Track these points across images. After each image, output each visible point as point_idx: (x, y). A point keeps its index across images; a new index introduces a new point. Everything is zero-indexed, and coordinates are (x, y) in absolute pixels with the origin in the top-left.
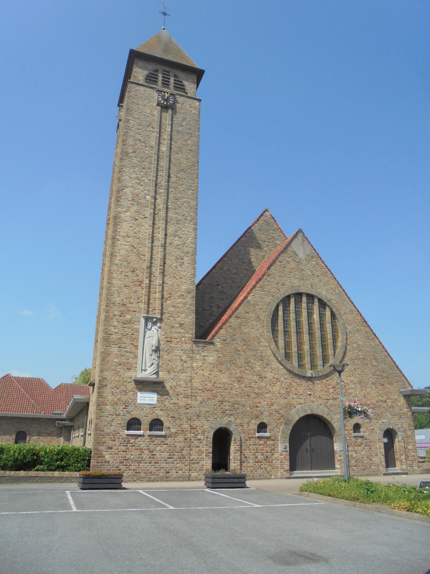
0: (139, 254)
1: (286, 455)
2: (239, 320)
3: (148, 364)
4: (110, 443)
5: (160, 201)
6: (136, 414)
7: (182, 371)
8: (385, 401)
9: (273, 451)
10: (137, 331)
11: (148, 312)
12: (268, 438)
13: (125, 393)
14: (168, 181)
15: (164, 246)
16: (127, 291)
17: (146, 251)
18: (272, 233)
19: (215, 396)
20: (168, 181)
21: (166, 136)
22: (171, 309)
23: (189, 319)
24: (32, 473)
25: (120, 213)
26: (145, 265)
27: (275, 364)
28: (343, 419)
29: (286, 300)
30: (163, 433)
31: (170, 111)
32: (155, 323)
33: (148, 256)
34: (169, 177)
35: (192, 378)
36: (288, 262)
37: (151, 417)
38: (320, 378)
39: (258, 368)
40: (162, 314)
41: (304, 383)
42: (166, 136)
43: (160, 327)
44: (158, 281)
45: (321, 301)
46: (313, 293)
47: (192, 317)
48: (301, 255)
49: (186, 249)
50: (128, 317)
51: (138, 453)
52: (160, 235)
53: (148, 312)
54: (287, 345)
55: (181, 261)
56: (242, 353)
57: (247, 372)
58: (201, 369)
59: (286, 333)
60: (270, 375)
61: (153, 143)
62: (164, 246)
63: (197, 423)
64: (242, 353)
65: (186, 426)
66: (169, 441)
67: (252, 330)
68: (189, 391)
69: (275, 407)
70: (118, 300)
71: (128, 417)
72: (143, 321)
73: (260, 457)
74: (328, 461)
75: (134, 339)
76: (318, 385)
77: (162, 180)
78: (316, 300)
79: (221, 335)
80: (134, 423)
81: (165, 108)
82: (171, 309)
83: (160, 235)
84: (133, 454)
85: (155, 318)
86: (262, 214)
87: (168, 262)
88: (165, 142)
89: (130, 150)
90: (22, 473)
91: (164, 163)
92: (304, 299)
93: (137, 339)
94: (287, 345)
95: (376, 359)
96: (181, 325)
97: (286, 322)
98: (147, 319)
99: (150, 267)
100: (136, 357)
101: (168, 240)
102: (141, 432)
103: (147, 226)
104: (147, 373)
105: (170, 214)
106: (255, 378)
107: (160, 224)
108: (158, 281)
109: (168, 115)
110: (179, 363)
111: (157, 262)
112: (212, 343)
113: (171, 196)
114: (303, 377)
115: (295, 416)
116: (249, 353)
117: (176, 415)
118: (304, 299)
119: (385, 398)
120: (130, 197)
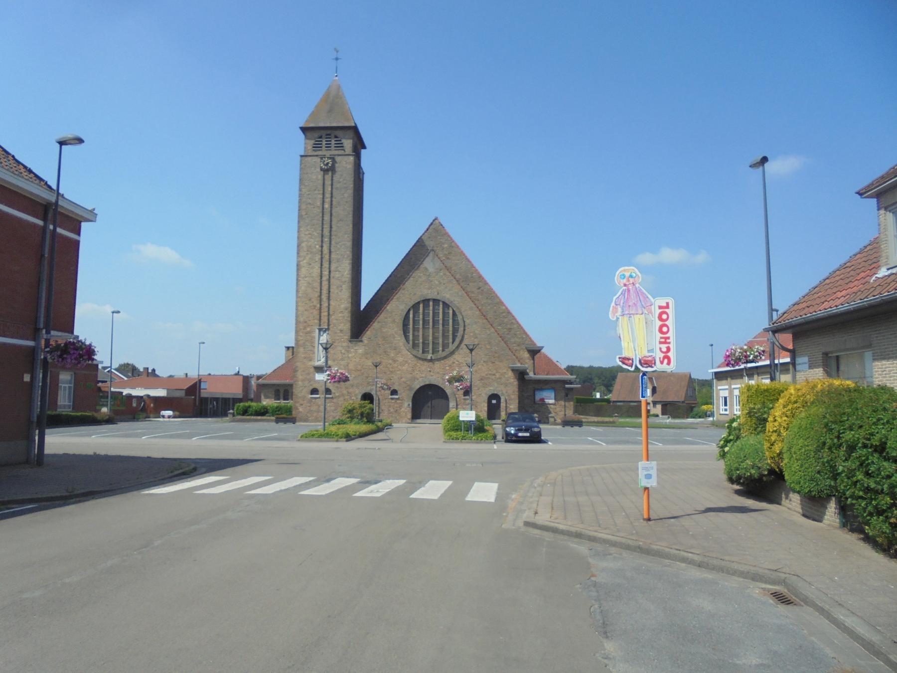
1: (410, 409)
4: (302, 402)
6: (316, 386)
7: (342, 360)
9: (400, 407)
10: (314, 337)
12: (398, 399)
13: (309, 374)
14: (331, 231)
19: (363, 374)
20: (331, 231)
21: (328, 195)
22: (335, 321)
24: (264, 418)
26: (317, 294)
27: (405, 352)
28: (474, 389)
29: (415, 307)
31: (330, 173)
32: (325, 332)
34: (331, 227)
36: (420, 277)
38: (439, 360)
40: (329, 325)
41: (426, 363)
42: (328, 195)
44: (325, 304)
45: (444, 303)
46: (438, 298)
50: (308, 329)
52: (326, 273)
54: (415, 337)
58: (353, 358)
59: (415, 329)
60: (400, 359)
61: (319, 203)
63: (351, 390)
65: (345, 392)
66: (335, 400)
71: (311, 388)
72: (317, 331)
73: (392, 410)
74: (819, 520)
76: (437, 365)
79: (368, 333)
80: (314, 391)
82: (335, 321)
83: (326, 273)
84: (314, 408)
88: (328, 200)
89: (304, 213)
90: (259, 417)
92: (431, 303)
93: (313, 342)
94: (415, 337)
95: (490, 343)
96: (341, 331)
97: (415, 322)
98: (320, 330)
99: (321, 295)
100: (314, 353)
101: (332, 275)
104: (321, 362)
105: (333, 256)
106: (390, 361)
107: (326, 265)
108: (325, 304)
109: (328, 177)
111: (325, 291)
113: (333, 242)
114: (425, 360)
115: (417, 386)
118: (431, 303)
119: (494, 372)
120: (305, 249)
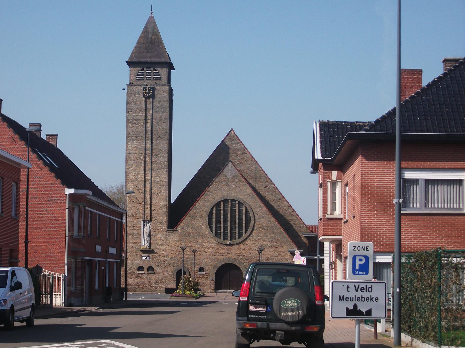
0: (139, 190)
2: (190, 218)
3: (146, 242)
4: (131, 277)
5: (148, 158)
8: (277, 256)
11: (144, 219)
15: (151, 184)
16: (134, 208)
17: (142, 187)
18: (235, 147)
21: (149, 117)
23: (165, 219)
25: (128, 169)
30: (153, 272)
32: (148, 223)
33: (143, 191)
35: (166, 248)
37: (148, 266)
39: (200, 241)
40: (151, 218)
43: (150, 225)
44: (148, 202)
47: (166, 218)
48: (229, 177)
49: (162, 183)
50: (135, 221)
51: (143, 280)
52: (148, 178)
53: (144, 219)
55: (159, 190)
56: (192, 234)
57: (194, 243)
60: (206, 245)
61: (142, 123)
62: (151, 184)
64: (192, 234)
66: (156, 276)
67: (198, 222)
68: (165, 254)
69: (209, 260)
70: (130, 214)
72: (142, 222)
75: (139, 231)
77: (149, 146)
78: (237, 202)
81: (147, 98)
82: (156, 215)
83: (148, 178)
85: (105, 268)
86: (228, 134)
87: (153, 191)
88: (149, 121)
91: (149, 135)
92: (230, 203)
102: (144, 272)
103: (142, 174)
105: (153, 165)
107: (148, 172)
109: (150, 101)
110: (160, 241)
111: (148, 192)
112: (177, 230)
116: (195, 234)
117: (159, 264)
